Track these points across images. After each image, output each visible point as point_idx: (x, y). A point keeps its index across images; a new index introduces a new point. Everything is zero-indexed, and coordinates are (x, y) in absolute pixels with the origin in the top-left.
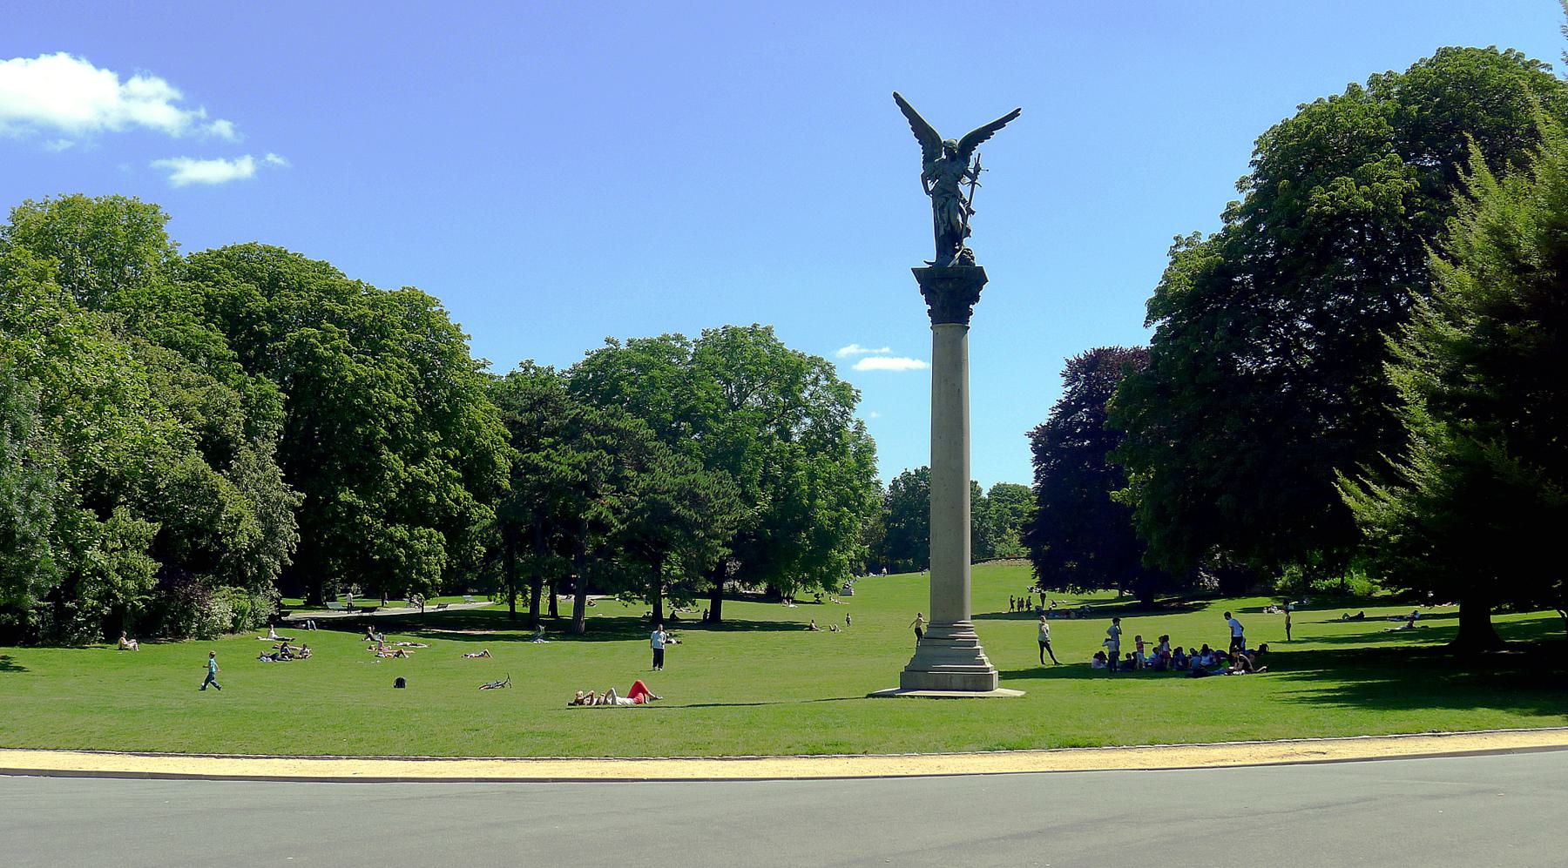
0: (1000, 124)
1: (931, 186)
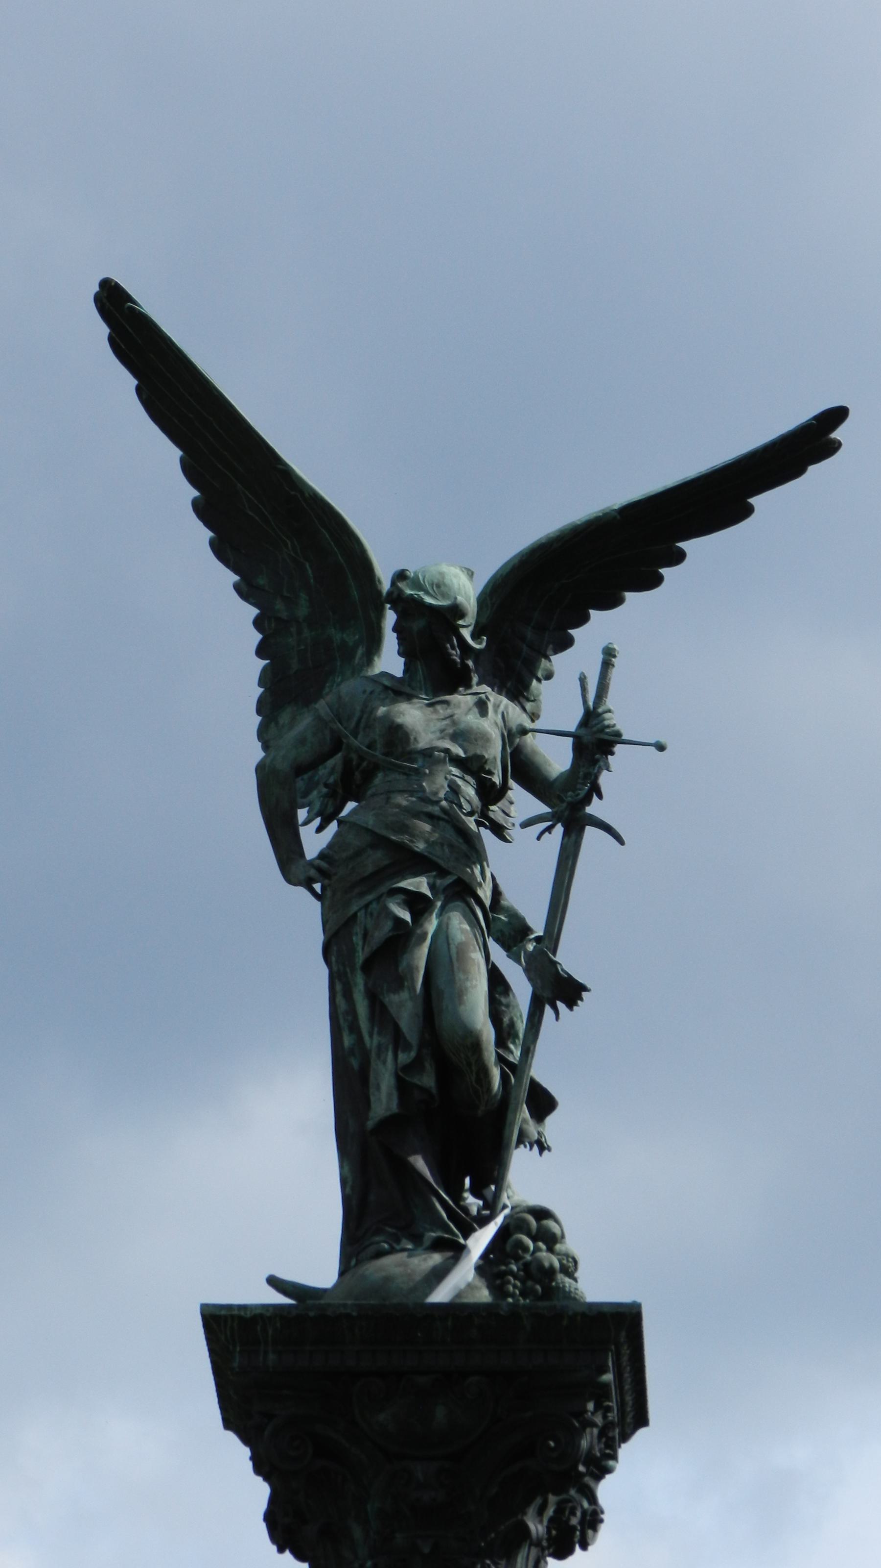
0: (718, 498)
1: (314, 841)
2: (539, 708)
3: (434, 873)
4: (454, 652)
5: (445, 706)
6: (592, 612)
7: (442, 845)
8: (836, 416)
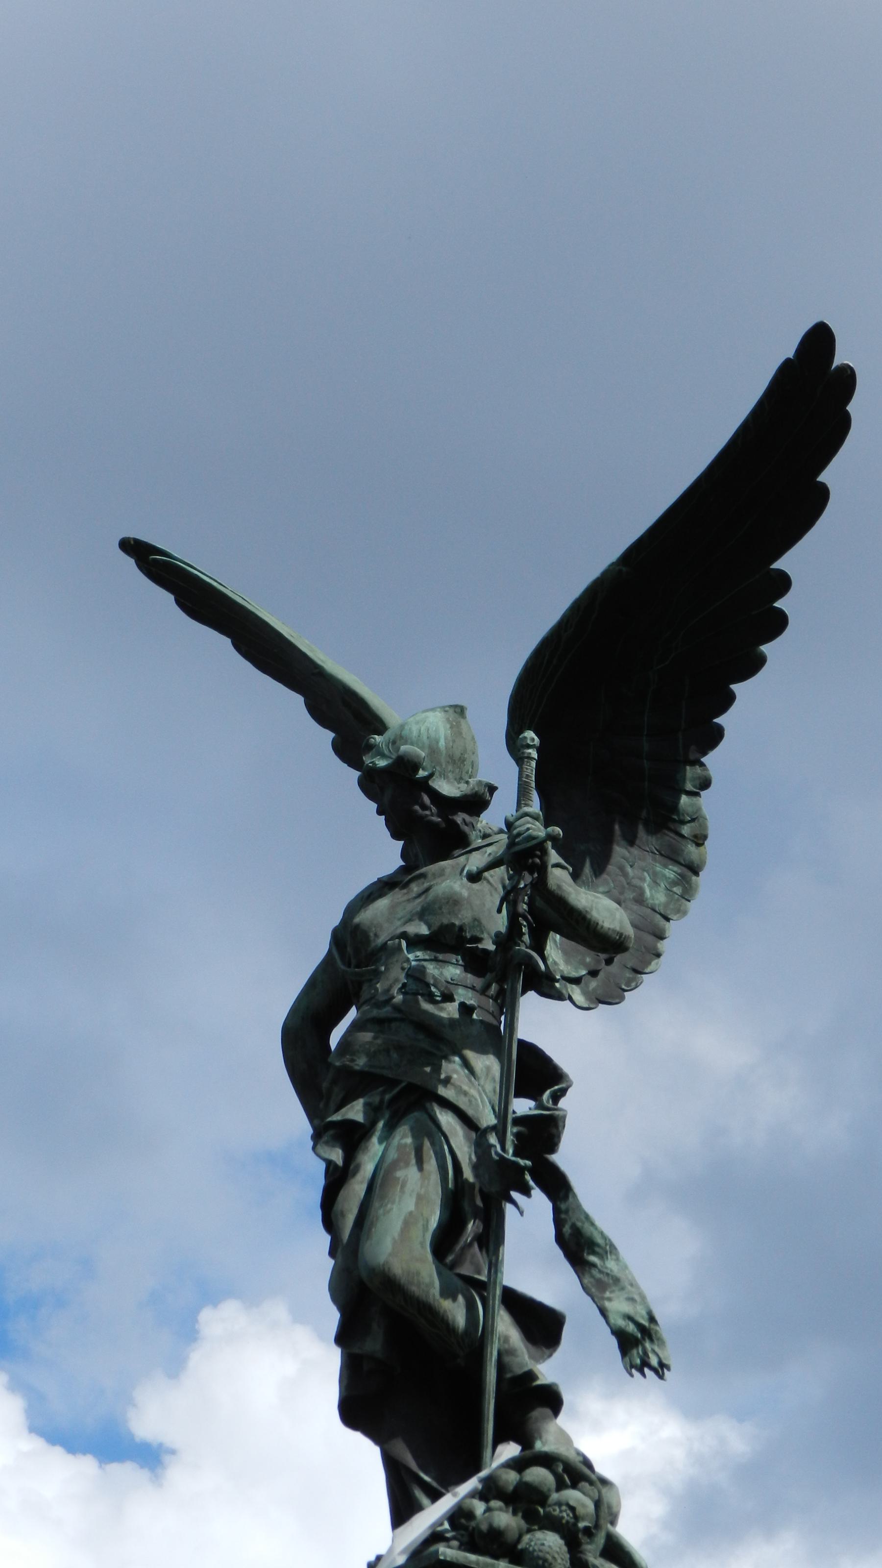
2: (704, 827)
3: (381, 1089)
4: (428, 812)
5: (422, 880)
6: (734, 687)
7: (387, 1051)
8: (819, 340)
